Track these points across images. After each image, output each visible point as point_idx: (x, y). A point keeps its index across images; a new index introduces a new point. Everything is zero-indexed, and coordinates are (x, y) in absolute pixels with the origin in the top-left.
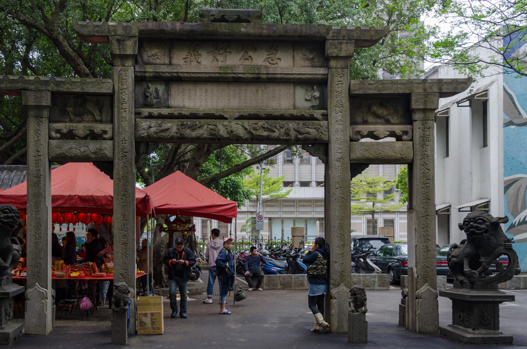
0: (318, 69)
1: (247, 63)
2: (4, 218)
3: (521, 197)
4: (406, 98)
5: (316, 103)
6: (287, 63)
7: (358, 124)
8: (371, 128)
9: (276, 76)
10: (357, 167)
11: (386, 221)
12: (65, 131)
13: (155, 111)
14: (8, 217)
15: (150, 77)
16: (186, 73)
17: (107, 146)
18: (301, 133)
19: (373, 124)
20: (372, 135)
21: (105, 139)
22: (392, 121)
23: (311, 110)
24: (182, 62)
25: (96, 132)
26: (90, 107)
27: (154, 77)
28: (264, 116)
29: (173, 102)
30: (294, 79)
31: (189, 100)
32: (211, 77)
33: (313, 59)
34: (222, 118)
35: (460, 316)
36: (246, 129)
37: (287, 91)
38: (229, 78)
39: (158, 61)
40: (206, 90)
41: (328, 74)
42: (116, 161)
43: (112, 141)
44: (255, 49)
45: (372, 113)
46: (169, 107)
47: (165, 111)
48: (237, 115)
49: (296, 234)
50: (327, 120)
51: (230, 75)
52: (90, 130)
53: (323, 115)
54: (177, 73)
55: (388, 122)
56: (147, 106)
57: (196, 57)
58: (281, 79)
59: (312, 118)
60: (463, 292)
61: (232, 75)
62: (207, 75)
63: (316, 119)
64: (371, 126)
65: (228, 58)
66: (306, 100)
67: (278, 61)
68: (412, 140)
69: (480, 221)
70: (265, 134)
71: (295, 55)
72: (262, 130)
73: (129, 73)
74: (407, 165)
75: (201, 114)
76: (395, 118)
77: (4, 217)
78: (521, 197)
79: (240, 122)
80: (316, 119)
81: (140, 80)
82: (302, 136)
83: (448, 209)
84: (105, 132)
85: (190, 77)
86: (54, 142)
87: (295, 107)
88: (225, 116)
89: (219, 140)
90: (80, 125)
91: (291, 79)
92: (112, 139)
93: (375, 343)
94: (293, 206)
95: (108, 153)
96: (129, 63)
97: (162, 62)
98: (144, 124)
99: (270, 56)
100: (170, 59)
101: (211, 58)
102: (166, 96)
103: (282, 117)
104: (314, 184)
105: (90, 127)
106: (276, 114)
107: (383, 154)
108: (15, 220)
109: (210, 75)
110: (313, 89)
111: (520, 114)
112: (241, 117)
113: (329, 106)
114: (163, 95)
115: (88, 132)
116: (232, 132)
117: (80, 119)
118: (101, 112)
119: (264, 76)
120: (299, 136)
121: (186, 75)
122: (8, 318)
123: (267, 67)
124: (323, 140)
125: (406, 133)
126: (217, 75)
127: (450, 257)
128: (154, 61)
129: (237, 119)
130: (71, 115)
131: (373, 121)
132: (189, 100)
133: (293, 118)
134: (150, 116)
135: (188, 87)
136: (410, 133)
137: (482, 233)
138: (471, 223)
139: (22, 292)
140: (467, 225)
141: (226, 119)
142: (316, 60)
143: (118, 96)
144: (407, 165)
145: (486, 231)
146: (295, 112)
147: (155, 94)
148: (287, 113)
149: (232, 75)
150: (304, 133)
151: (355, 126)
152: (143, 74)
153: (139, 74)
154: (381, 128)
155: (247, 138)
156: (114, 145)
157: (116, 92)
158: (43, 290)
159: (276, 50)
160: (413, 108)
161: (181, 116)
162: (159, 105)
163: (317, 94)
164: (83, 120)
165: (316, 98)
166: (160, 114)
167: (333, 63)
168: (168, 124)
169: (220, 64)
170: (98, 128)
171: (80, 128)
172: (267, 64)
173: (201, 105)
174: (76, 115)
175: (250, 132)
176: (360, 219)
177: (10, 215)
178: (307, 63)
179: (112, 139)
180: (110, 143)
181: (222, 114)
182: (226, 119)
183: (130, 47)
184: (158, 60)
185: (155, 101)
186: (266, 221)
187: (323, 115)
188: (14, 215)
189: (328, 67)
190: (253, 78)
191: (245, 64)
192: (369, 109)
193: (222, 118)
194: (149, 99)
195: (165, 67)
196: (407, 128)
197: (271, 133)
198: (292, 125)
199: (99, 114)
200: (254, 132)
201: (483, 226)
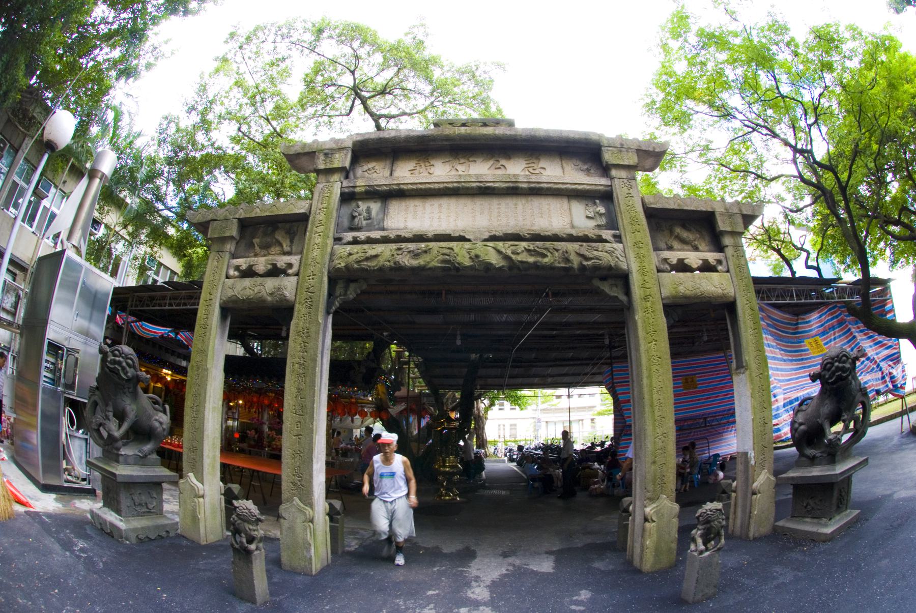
1: (499, 172)
5: (603, 221)
6: (553, 172)
9: (542, 185)
12: (244, 267)
13: (362, 235)
15: (361, 193)
16: (411, 184)
18: (587, 259)
21: (288, 275)
22: (700, 248)
24: (408, 174)
25: (279, 266)
28: (528, 236)
30: (567, 189)
32: (447, 188)
34: (462, 239)
37: (559, 205)
38: (472, 188)
40: (440, 205)
42: (297, 306)
43: (296, 278)
44: (508, 157)
46: (383, 229)
48: (486, 235)
50: (621, 242)
51: (474, 185)
52: (273, 264)
54: (398, 184)
55: (696, 249)
56: (352, 229)
58: (549, 189)
60: (821, 471)
61: (478, 184)
62: (441, 186)
63: (606, 241)
65: (472, 167)
66: (588, 217)
67: (542, 171)
68: (728, 271)
70: (531, 260)
71: (564, 165)
72: (525, 253)
75: (430, 235)
76: (703, 245)
79: (491, 244)
80: (606, 241)
82: (589, 263)
84: (290, 265)
85: (417, 190)
86: (230, 282)
87: (573, 227)
88: (467, 237)
90: (262, 260)
91: (562, 190)
92: (297, 274)
95: (289, 294)
96: (336, 177)
98: (342, 250)
102: (381, 216)
103: (556, 238)
106: (547, 234)
107: (698, 291)
109: (446, 185)
112: (493, 238)
113: (620, 224)
114: (377, 214)
115: (270, 267)
116: (477, 256)
120: (585, 263)
121: (410, 187)
124: (621, 269)
125: (719, 262)
126: (455, 185)
127: (796, 425)
129: (485, 240)
130: (257, 248)
132: (406, 218)
133: (571, 238)
134: (355, 241)
141: (469, 240)
146: (574, 232)
147: (365, 214)
148: (561, 234)
149: (478, 184)
150: (592, 259)
153: (346, 190)
155: (503, 266)
157: (312, 212)
159: (538, 158)
160: (722, 229)
161: (399, 239)
162: (370, 228)
164: (269, 254)
165: (601, 215)
166: (368, 238)
167: (614, 172)
168: (378, 249)
171: (261, 263)
173: (431, 225)
174: (261, 248)
175: (506, 257)
179: (297, 274)
180: (294, 279)
181: (462, 234)
182: (469, 240)
184: (376, 174)
185: (364, 223)
186: (544, 424)
187: (615, 236)
190: (508, 188)
192: (671, 232)
193: (462, 239)
194: (356, 220)
197: (540, 259)
198: (572, 247)
199: (289, 243)
200: (513, 257)
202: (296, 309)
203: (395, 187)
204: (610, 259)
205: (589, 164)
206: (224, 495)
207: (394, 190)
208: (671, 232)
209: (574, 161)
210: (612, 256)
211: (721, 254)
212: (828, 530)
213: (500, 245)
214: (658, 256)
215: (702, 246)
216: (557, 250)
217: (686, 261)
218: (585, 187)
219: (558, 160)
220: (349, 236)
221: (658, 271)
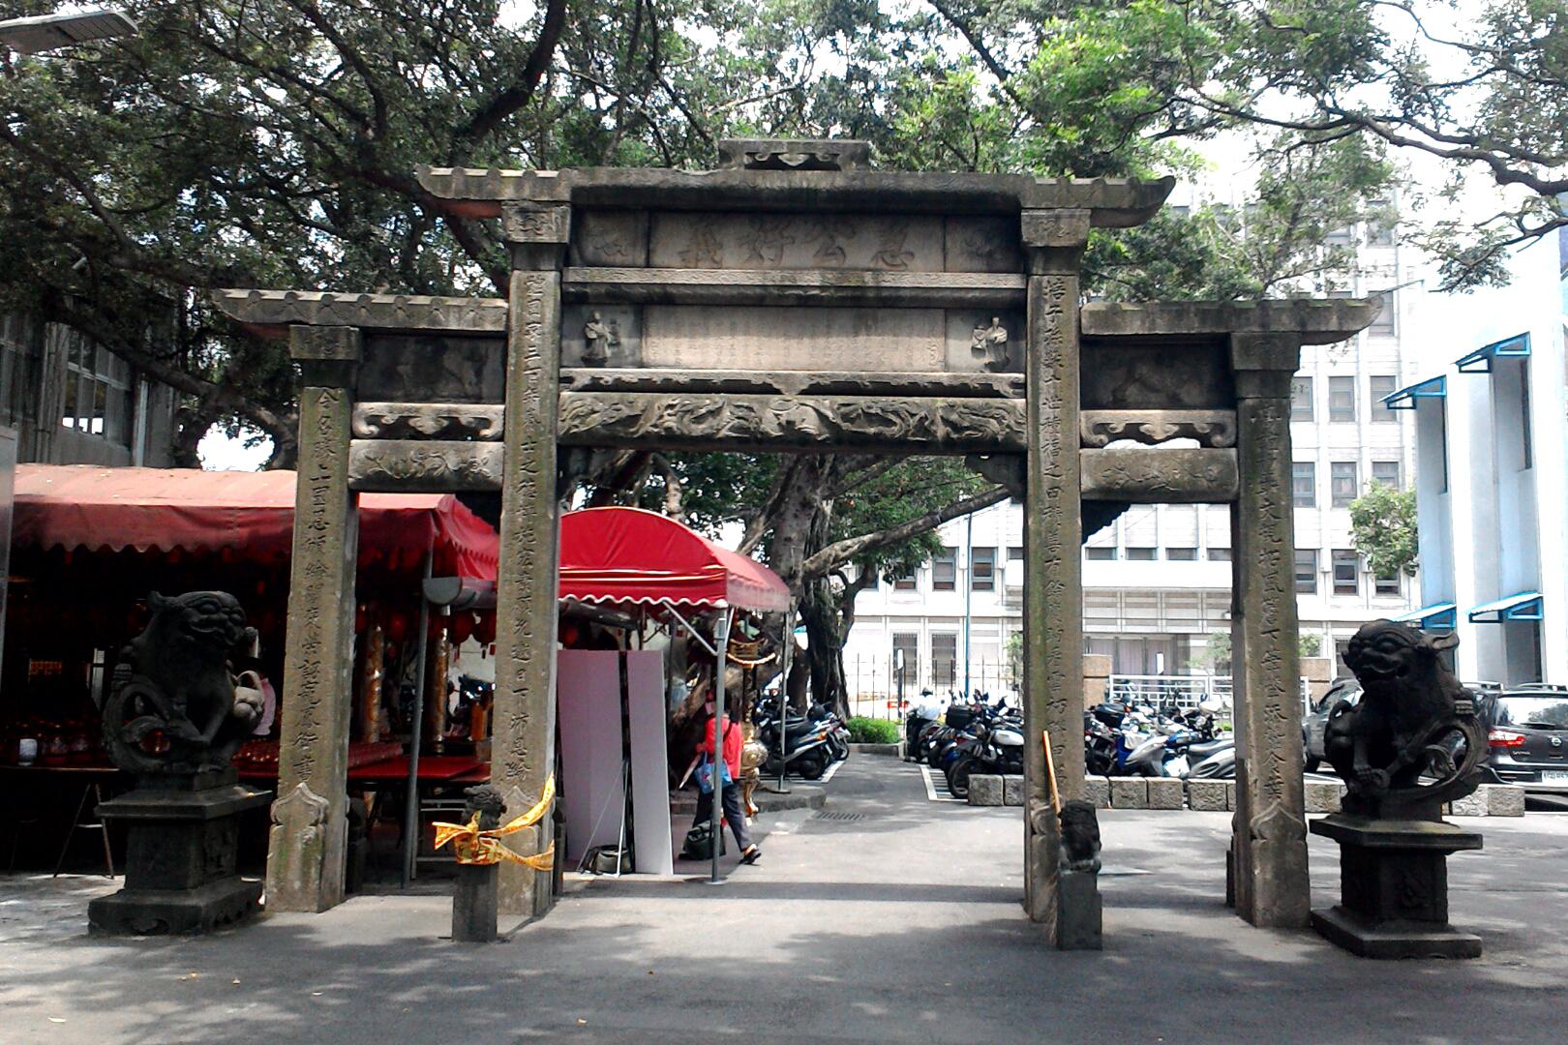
0: (1001, 276)
2: (202, 624)
4: (1220, 345)
8: (1134, 415)
10: (1101, 509)
11: (936, 640)
13: (608, 374)
15: (598, 296)
17: (486, 455)
20: (1133, 432)
21: (485, 439)
22: (1186, 399)
23: (988, 373)
26: (450, 361)
27: (609, 295)
33: (990, 255)
34: (767, 389)
41: (1025, 290)
47: (631, 374)
53: (1014, 385)
56: (589, 361)
58: (912, 299)
59: (988, 391)
62: (735, 292)
63: (998, 394)
65: (787, 251)
69: (1387, 644)
71: (949, 244)
73: (545, 284)
76: (1195, 392)
79: (811, 400)
80: (998, 394)
81: (574, 303)
84: (486, 423)
85: (694, 296)
89: (759, 442)
94: (1194, 606)
97: (629, 260)
100: (649, 254)
103: (913, 389)
104: (1162, 553)
105: (449, 411)
108: (229, 630)
115: (445, 423)
119: (871, 294)
122: (213, 869)
125: (1219, 428)
129: (803, 392)
132: (682, 353)
133: (938, 390)
134: (595, 386)
136: (1231, 429)
137: (1393, 674)
138: (1367, 650)
139: (261, 803)
142: (998, 256)
143: (519, 339)
145: (1403, 670)
146: (944, 377)
154: (1154, 419)
161: (669, 387)
170: (468, 412)
171: (427, 414)
177: (215, 616)
179: (500, 438)
182: (778, 392)
183: (553, 229)
185: (608, 352)
189: (1027, 274)
193: (767, 389)
196: (1225, 416)
199: (474, 380)
200: (845, 426)
201: (1394, 657)
202: (505, 497)
206: (348, 816)
211: (1228, 413)
212: (1367, 937)
213: (827, 404)
216: (913, 415)
218: (977, 294)
221: (1084, 445)
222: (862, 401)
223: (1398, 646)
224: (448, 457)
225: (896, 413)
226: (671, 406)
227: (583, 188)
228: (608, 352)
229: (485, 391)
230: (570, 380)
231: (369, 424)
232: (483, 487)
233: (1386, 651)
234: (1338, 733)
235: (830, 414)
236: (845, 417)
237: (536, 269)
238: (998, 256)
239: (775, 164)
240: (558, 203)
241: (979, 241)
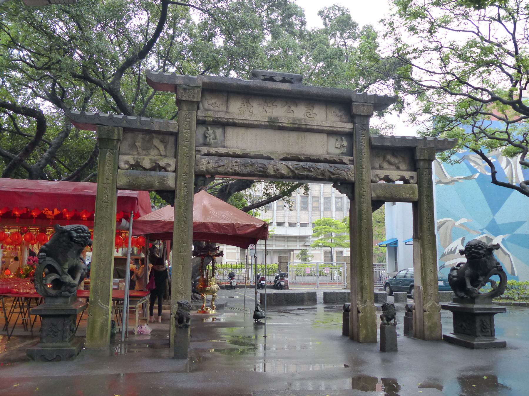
0: (346, 124)
1: (290, 115)
2: (77, 237)
3: (448, 234)
5: (344, 150)
6: (322, 117)
7: (376, 169)
9: (313, 127)
13: (213, 150)
14: (80, 237)
16: (241, 119)
19: (387, 169)
22: (401, 168)
24: (236, 111)
27: (213, 121)
28: (303, 158)
29: (227, 143)
31: (238, 141)
33: (341, 116)
35: (462, 326)
36: (290, 168)
39: (217, 109)
42: (178, 192)
43: (174, 173)
45: (387, 161)
47: (221, 151)
48: (281, 157)
49: (282, 261)
53: (350, 160)
55: (398, 168)
56: (205, 144)
57: (249, 108)
59: (342, 163)
64: (387, 171)
67: (314, 116)
70: (305, 173)
71: (328, 112)
74: (411, 204)
76: (404, 166)
77: (77, 236)
78: (448, 234)
79: (284, 163)
80: (344, 163)
83: (396, 243)
84: (169, 165)
88: (272, 157)
93: (512, 348)
97: (220, 109)
99: (308, 111)
101: (261, 109)
102: (222, 138)
104: (287, 225)
105: (155, 160)
108: (87, 240)
109: (260, 123)
110: (342, 139)
111: (446, 176)
115: (154, 164)
116: (278, 170)
117: (147, 153)
118: (165, 147)
119: (304, 127)
120: (332, 177)
123: (305, 120)
125: (412, 177)
128: (214, 109)
129: (281, 160)
130: (140, 150)
131: (387, 167)
132: (238, 141)
134: (209, 154)
135: (241, 131)
136: (415, 178)
138: (473, 249)
140: (469, 251)
141: (272, 159)
144: (411, 204)
146: (328, 157)
147: (213, 136)
151: (374, 170)
152: (204, 118)
153: (201, 118)
156: (176, 177)
158: (105, 306)
162: (216, 145)
163: (345, 143)
164: (150, 154)
165: (344, 147)
168: (225, 161)
169: (268, 114)
172: (306, 117)
175: (292, 171)
176: (320, 250)
177: (82, 234)
178: (337, 119)
181: (269, 155)
182: (272, 159)
184: (213, 107)
185: (213, 141)
187: (350, 160)
188: (86, 235)
191: (288, 116)
192: (384, 158)
193: (269, 158)
194: (208, 139)
195: (222, 113)
196: (414, 174)
199: (164, 149)
200: (296, 171)
203: (231, 120)
204: (346, 175)
205: (343, 112)
207: (230, 122)
208: (384, 158)
209: (334, 109)
210: (347, 173)
213: (289, 163)
214: (373, 173)
215: (403, 166)
216: (319, 169)
217: (389, 177)
219: (324, 108)
220: (204, 150)
221: (372, 182)
222: (302, 164)
223: (483, 248)
224: (155, 177)
225: (313, 168)
226: (236, 162)
227: (206, 83)
228: (213, 141)
229: (168, 154)
230: (199, 151)
231: (125, 164)
232: (169, 189)
233: (479, 249)
234: (454, 277)
235: (292, 168)
236: (296, 169)
237: (270, 118)
238: (343, 117)
239: (271, 79)
240: (197, 87)
241: (337, 111)
